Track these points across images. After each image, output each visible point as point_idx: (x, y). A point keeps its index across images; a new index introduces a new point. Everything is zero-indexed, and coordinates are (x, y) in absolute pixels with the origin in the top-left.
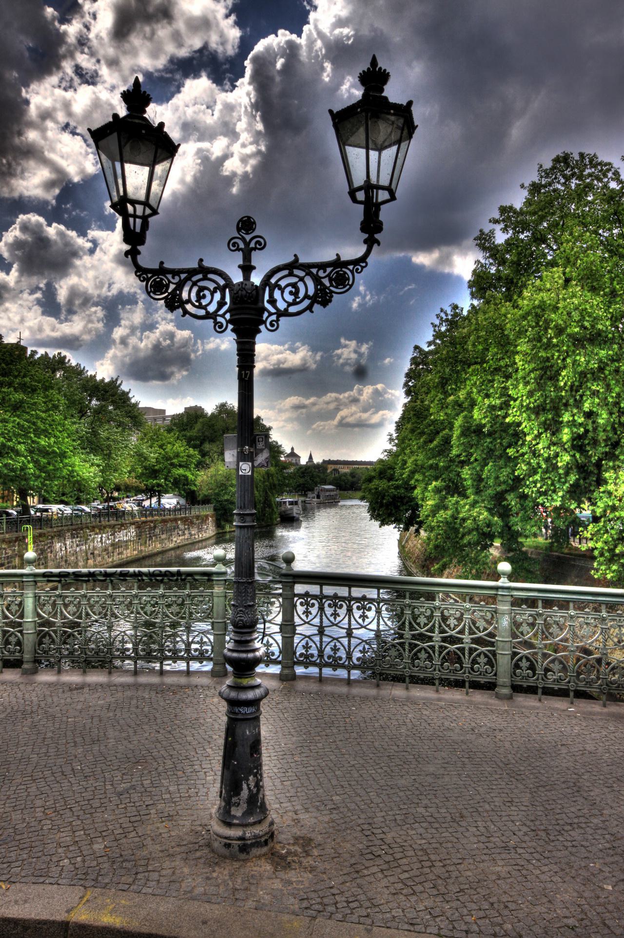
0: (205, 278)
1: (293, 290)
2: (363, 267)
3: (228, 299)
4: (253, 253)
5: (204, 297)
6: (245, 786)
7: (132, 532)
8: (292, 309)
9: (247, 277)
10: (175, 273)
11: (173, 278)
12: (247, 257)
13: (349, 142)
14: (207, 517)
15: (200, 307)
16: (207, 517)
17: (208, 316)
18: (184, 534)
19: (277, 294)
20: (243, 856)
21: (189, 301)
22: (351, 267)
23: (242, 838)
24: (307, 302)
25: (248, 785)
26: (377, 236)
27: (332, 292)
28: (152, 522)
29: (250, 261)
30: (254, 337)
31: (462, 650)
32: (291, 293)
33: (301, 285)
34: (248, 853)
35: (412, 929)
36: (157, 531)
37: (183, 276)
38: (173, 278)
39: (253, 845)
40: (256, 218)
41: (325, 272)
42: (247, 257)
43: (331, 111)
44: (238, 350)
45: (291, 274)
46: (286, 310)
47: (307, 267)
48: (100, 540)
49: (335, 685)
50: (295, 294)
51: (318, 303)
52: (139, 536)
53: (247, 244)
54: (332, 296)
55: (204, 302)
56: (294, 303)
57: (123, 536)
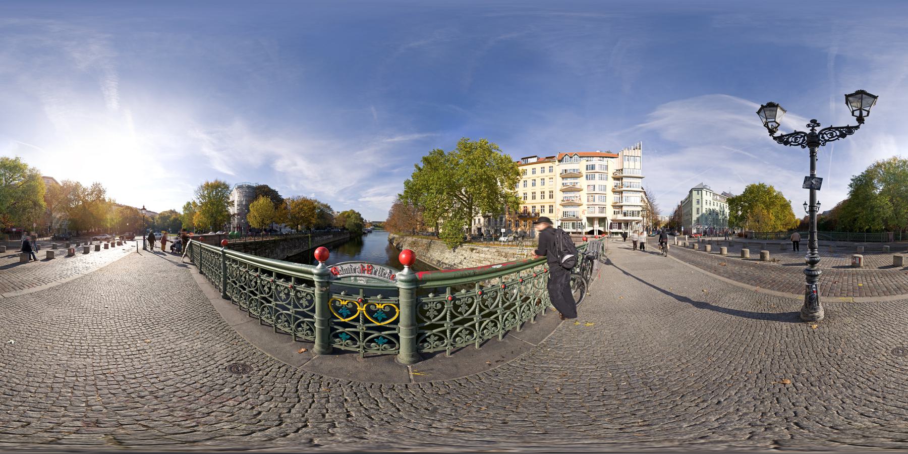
3: (806, 139)
7: (332, 236)
15: (796, 142)
17: (799, 144)
19: (825, 135)
21: (792, 141)
31: (357, 334)
32: (830, 135)
35: (173, 423)
48: (325, 237)
49: (485, 271)
52: (333, 236)
57: (329, 237)
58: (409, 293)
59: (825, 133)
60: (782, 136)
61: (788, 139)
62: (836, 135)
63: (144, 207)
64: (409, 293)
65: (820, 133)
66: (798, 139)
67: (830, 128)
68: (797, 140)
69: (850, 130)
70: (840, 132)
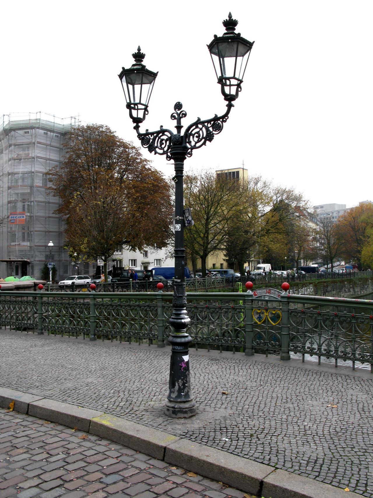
0: (163, 135)
1: (197, 135)
2: (226, 119)
4: (182, 119)
5: (163, 144)
6: (177, 384)
8: (198, 145)
9: (179, 131)
10: (152, 134)
11: (151, 136)
12: (179, 122)
13: (226, 56)
14: (367, 280)
16: (367, 280)
18: (349, 291)
20: (174, 416)
22: (221, 120)
23: (173, 407)
24: (203, 140)
25: (178, 384)
26: (233, 102)
27: (213, 134)
28: (325, 282)
29: (180, 124)
30: (183, 161)
32: (197, 137)
33: (201, 132)
34: (176, 415)
36: (329, 288)
37: (155, 135)
38: (151, 136)
39: (178, 411)
40: (182, 102)
41: (210, 124)
42: (179, 122)
43: (207, 45)
44: (175, 168)
45: (197, 127)
46: (195, 146)
47: (203, 123)
50: (198, 137)
51: (208, 140)
53: (178, 115)
54: (214, 136)
55: (163, 146)
56: (199, 141)
61: (154, 140)
63: (139, 56)
67: (196, 124)
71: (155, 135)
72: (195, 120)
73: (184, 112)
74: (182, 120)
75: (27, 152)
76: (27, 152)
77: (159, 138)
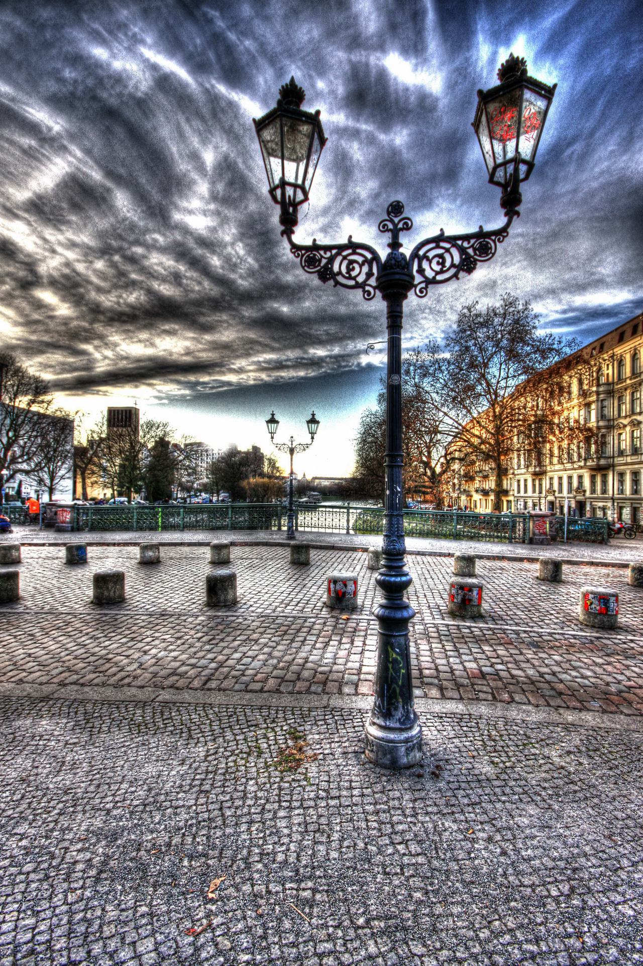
3: (375, 270)
17: (358, 286)
19: (425, 265)
27: (476, 260)
32: (438, 263)
37: (334, 252)
45: (438, 247)
51: (463, 270)
56: (442, 272)
58: (462, 205)
59: (425, 257)
60: (315, 247)
61: (331, 260)
62: (453, 265)
64: (462, 205)
65: (415, 254)
66: (356, 266)
68: (353, 269)
69: (308, 446)
70: (462, 250)
71: (334, 252)
72: (437, 233)
73: (410, 223)
74: (401, 234)
75: (292, 171)
76: (292, 171)
77: (345, 258)
